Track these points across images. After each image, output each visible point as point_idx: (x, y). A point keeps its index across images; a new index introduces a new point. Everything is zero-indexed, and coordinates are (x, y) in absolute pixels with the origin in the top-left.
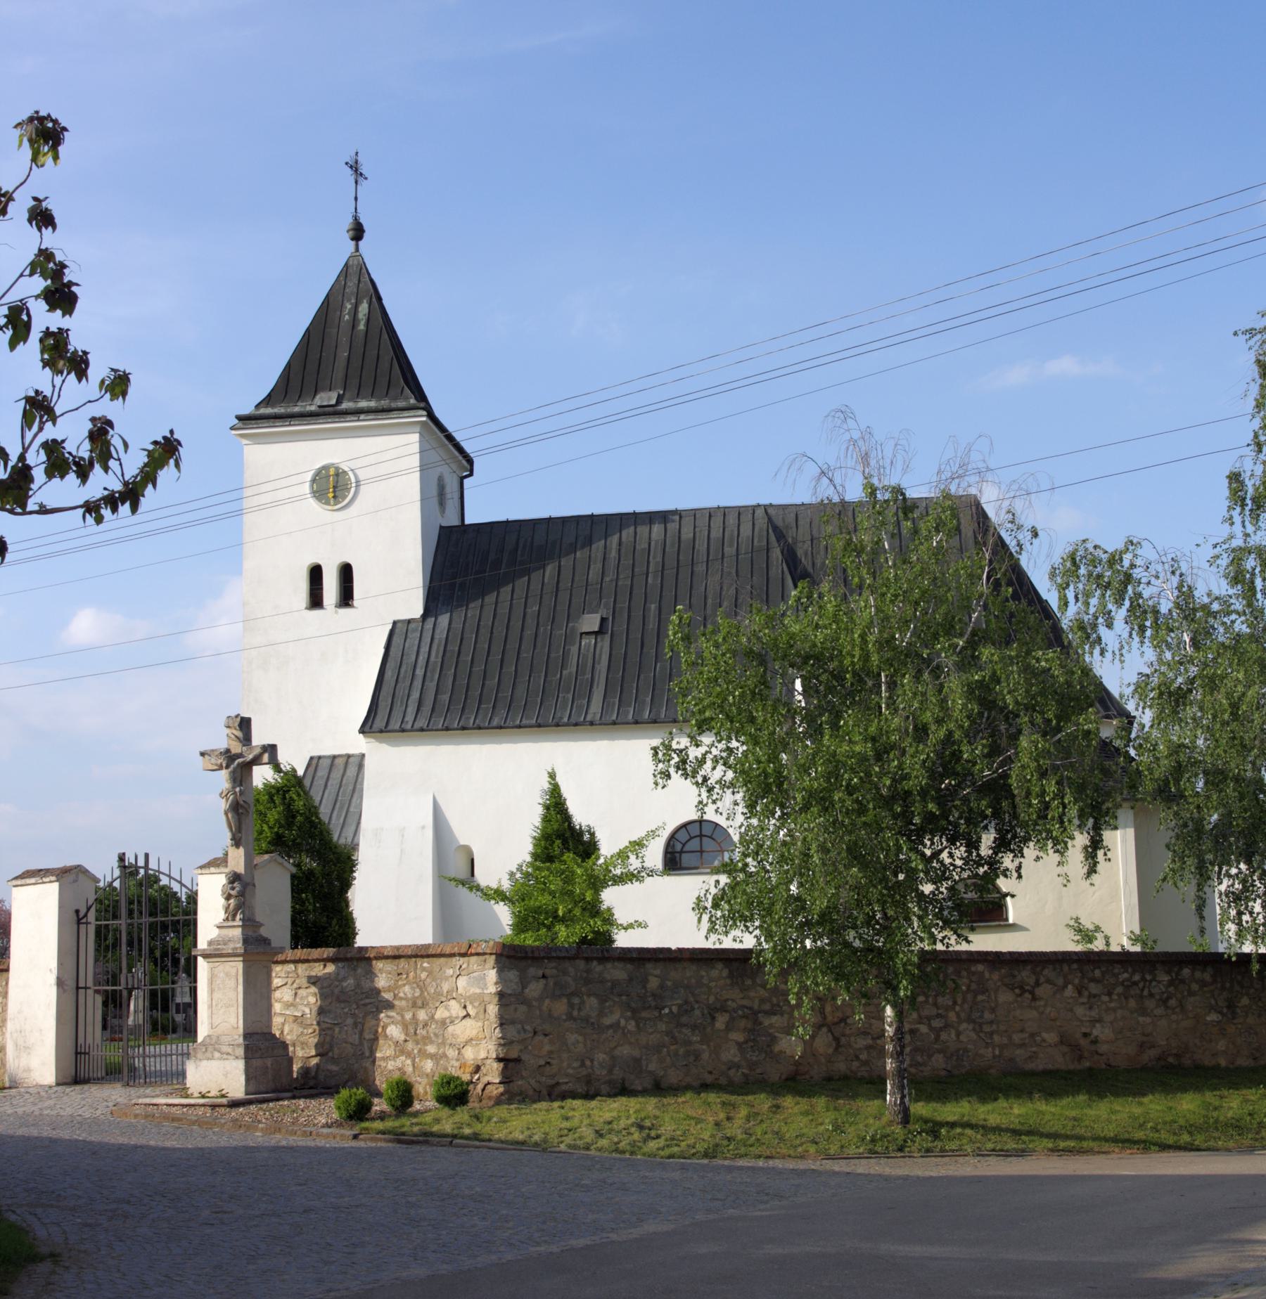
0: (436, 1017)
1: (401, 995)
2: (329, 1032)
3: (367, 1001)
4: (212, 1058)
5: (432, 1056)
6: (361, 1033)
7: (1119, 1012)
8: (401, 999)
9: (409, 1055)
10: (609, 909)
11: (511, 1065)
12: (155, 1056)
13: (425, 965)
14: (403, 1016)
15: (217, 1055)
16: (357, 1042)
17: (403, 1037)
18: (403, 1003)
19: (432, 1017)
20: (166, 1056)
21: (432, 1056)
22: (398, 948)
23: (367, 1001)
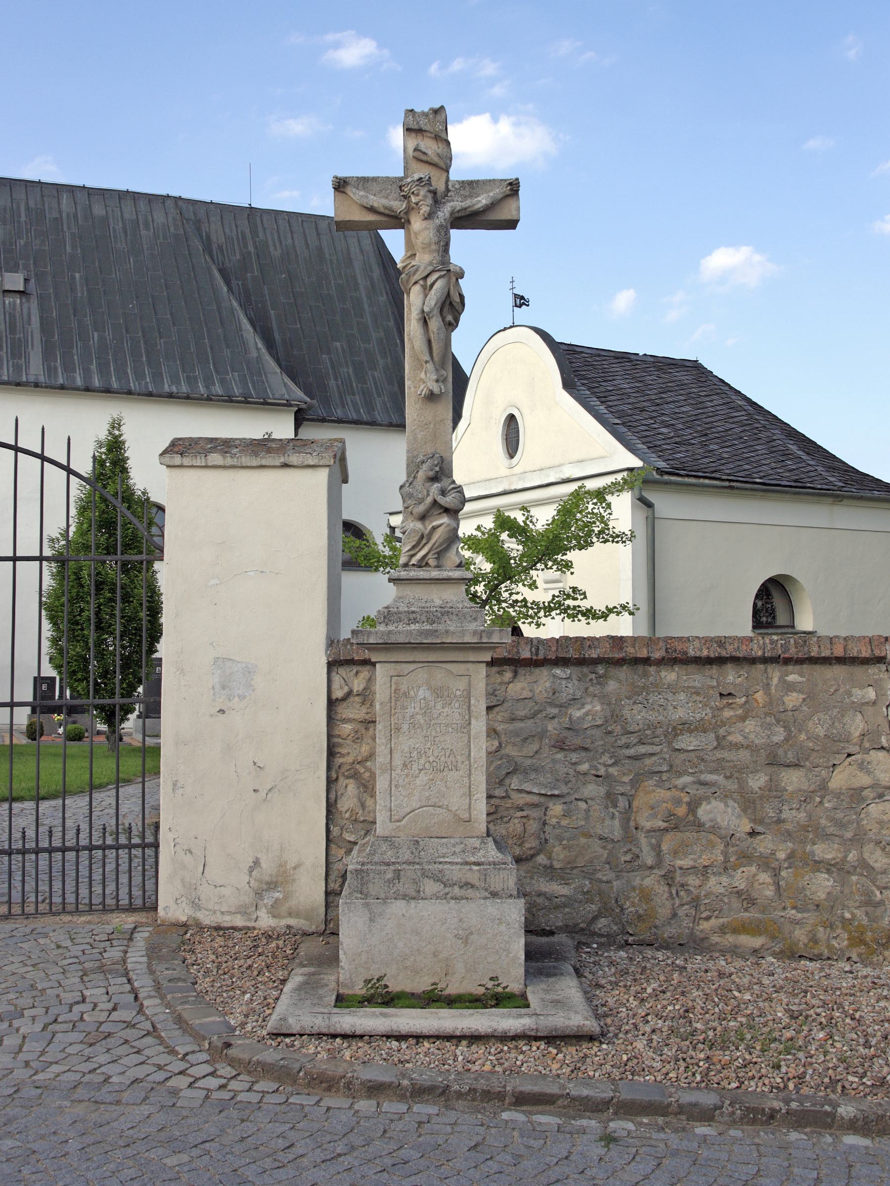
0: (834, 784)
1: (736, 738)
2: (535, 813)
3: (642, 749)
4: (417, 896)
5: (829, 867)
6: (627, 814)
7: (461, 606)
8: (737, 746)
9: (766, 863)
10: (144, 493)
11: (147, 733)
12: (77, 849)
13: (792, 678)
14: (742, 783)
15: (431, 887)
16: (617, 834)
17: (746, 826)
18: (744, 756)
19: (823, 787)
20: (104, 848)
21: (829, 867)
22: (721, 642)
23: (642, 749)
